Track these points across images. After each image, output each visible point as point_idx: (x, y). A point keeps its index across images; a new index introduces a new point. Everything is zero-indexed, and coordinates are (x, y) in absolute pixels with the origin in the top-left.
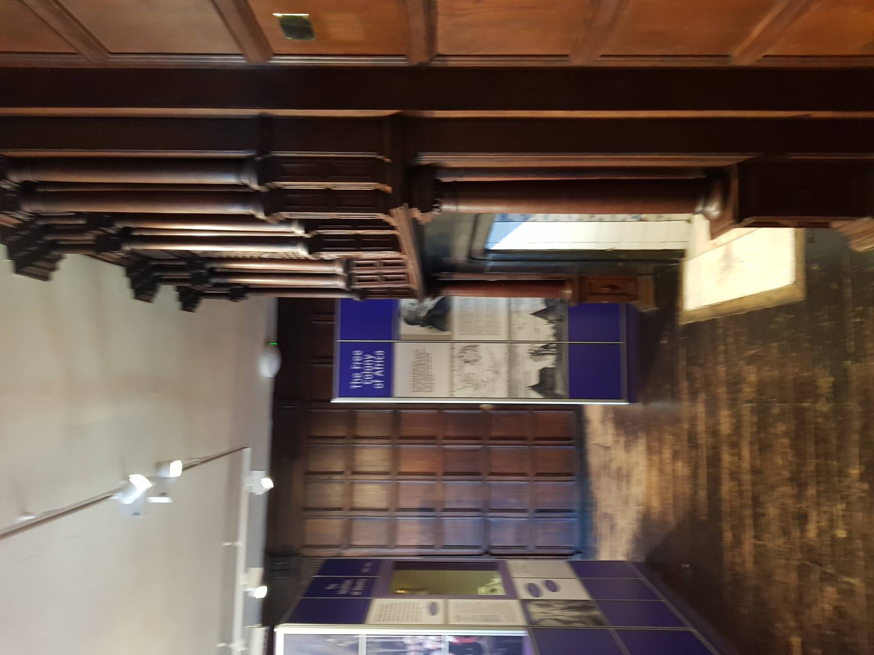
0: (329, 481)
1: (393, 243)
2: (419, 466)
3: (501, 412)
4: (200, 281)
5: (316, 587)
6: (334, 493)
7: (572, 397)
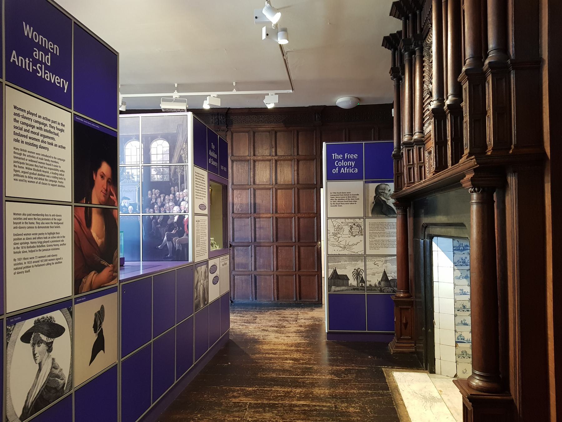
1: (441, 165)
2: (281, 202)
3: (316, 255)
4: (405, 48)
5: (213, 137)
6: (264, 151)
7: (330, 297)
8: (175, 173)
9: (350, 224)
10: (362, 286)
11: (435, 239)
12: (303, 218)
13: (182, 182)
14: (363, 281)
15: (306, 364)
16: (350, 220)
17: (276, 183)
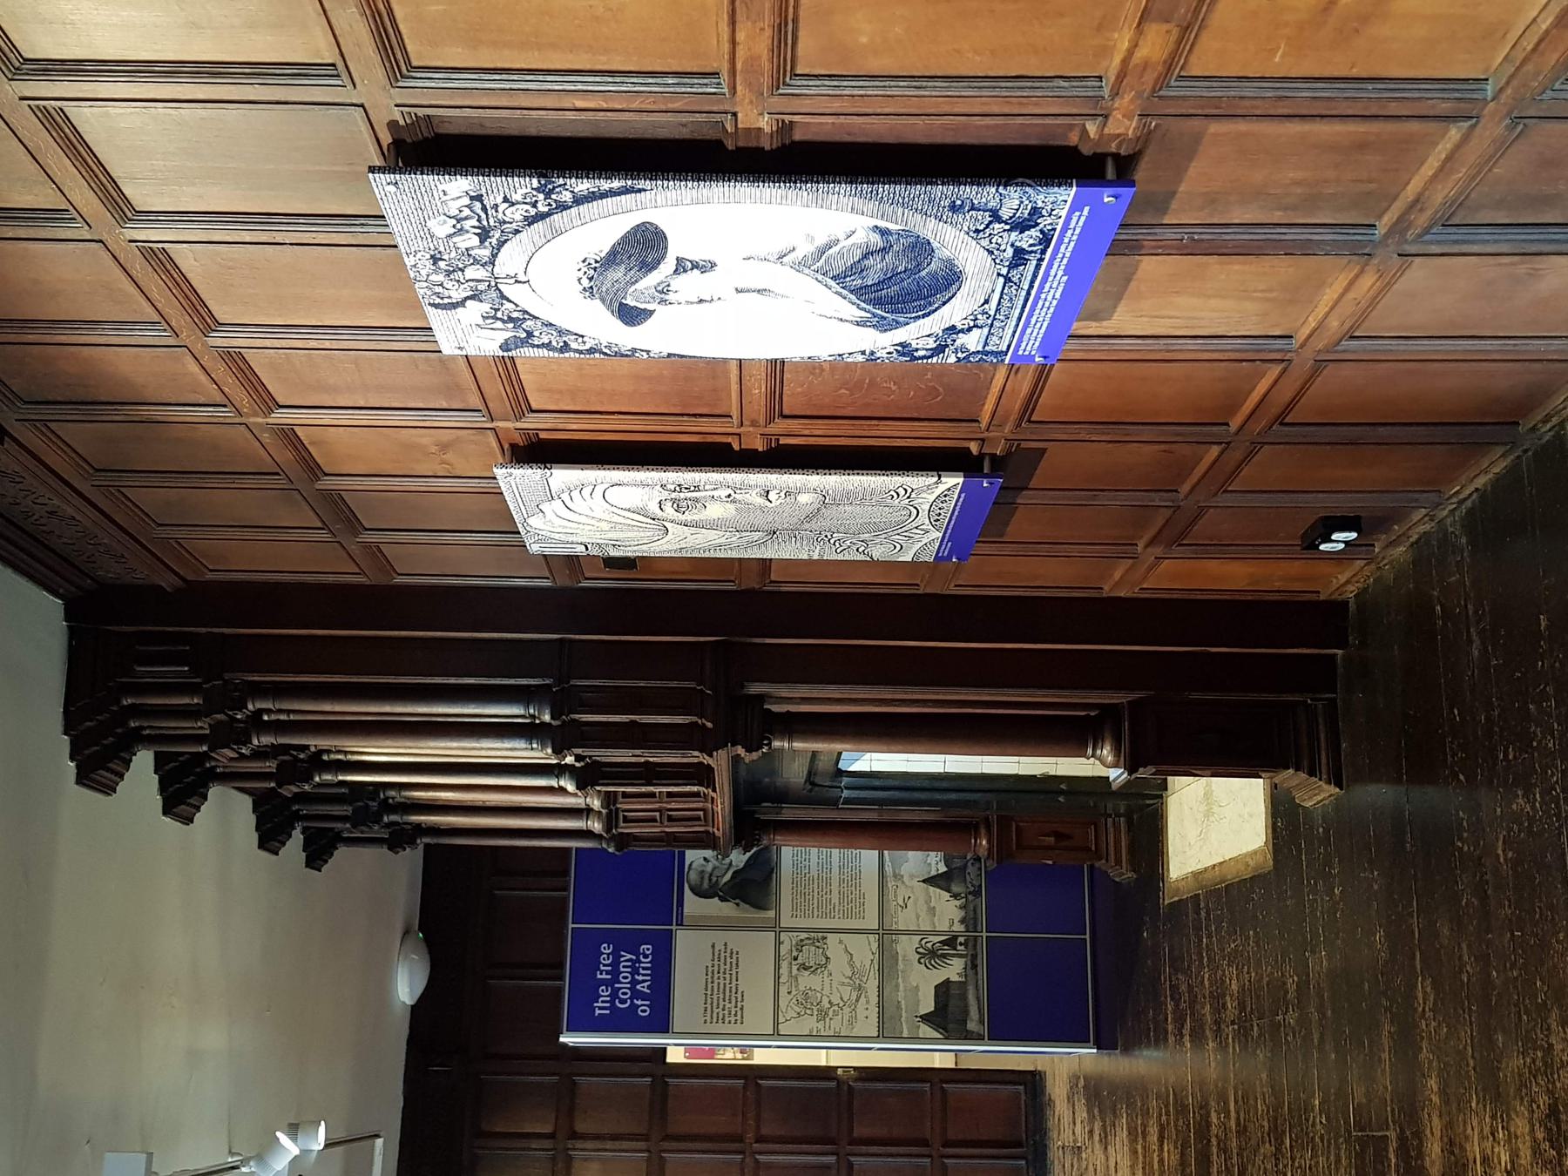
9: (795, 971)
10: (965, 944)
12: (758, 1127)
14: (951, 942)
15: (1167, 1106)
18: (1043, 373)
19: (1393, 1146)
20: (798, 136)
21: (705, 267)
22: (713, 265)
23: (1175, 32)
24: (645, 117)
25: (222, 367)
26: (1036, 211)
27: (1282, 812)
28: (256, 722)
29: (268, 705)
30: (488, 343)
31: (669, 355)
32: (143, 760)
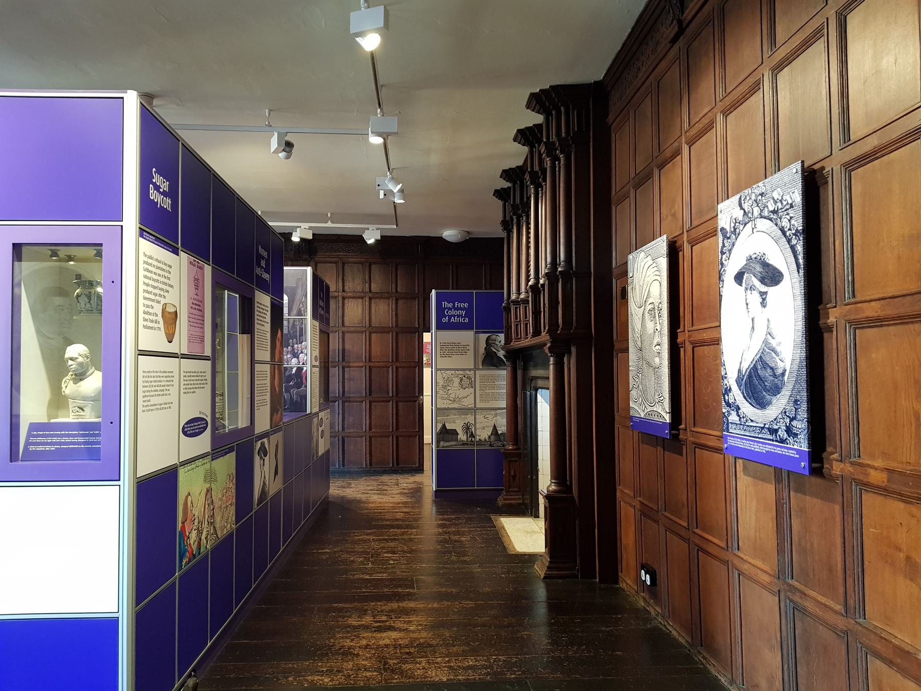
0: (364, 282)
2: (376, 349)
8: (294, 325)
11: (540, 390)
13: (301, 335)
14: (472, 435)
16: (460, 372)
17: (370, 326)
18: (718, 450)
19: (411, 591)
20: (826, 335)
21: (763, 304)
22: (764, 307)
23: (884, 485)
24: (832, 270)
25: (706, 122)
26: (796, 435)
27: (528, 559)
28: (555, 159)
29: (562, 162)
30: (724, 222)
31: (721, 296)
32: (539, 119)
